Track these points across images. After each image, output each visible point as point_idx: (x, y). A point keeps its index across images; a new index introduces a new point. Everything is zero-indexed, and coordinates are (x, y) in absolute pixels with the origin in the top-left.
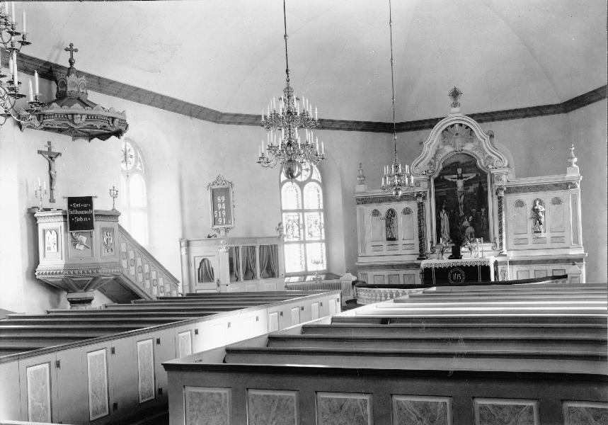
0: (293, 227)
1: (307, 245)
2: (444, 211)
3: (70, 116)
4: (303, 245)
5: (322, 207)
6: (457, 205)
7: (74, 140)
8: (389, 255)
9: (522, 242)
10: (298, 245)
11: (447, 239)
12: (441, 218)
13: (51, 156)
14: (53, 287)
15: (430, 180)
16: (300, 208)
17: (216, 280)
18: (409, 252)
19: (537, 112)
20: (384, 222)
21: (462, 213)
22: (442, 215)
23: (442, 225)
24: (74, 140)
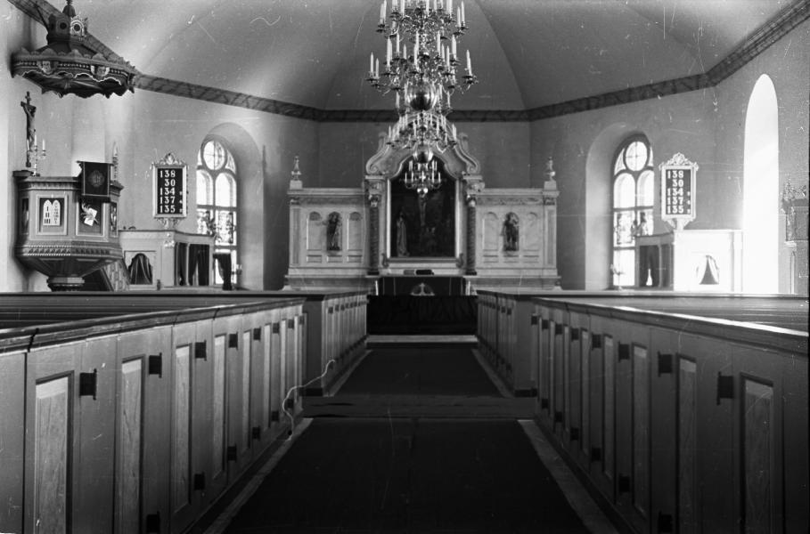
0: (202, 226)
1: (633, 205)
2: (401, 220)
3: (92, 68)
4: (639, 205)
5: (234, 205)
6: (418, 214)
7: (43, 92)
8: (329, 267)
9: (491, 259)
10: (623, 206)
11: (403, 252)
12: (397, 227)
13: (30, 111)
14: (54, 267)
15: (386, 182)
16: (211, 203)
17: (154, 281)
18: (354, 265)
19: (497, 116)
20: (324, 228)
21: (423, 224)
22: (398, 224)
23: (399, 235)
24: (43, 92)
